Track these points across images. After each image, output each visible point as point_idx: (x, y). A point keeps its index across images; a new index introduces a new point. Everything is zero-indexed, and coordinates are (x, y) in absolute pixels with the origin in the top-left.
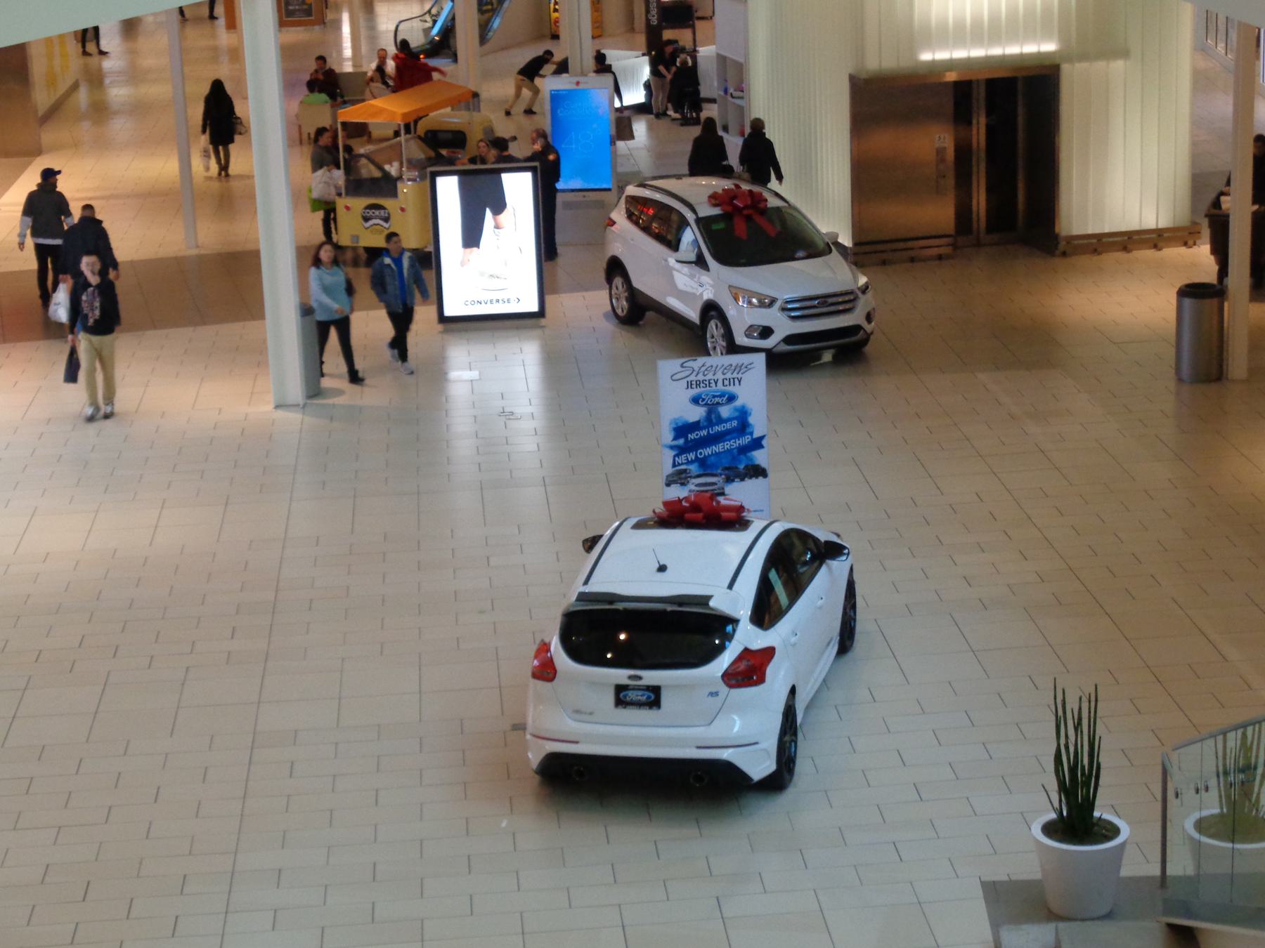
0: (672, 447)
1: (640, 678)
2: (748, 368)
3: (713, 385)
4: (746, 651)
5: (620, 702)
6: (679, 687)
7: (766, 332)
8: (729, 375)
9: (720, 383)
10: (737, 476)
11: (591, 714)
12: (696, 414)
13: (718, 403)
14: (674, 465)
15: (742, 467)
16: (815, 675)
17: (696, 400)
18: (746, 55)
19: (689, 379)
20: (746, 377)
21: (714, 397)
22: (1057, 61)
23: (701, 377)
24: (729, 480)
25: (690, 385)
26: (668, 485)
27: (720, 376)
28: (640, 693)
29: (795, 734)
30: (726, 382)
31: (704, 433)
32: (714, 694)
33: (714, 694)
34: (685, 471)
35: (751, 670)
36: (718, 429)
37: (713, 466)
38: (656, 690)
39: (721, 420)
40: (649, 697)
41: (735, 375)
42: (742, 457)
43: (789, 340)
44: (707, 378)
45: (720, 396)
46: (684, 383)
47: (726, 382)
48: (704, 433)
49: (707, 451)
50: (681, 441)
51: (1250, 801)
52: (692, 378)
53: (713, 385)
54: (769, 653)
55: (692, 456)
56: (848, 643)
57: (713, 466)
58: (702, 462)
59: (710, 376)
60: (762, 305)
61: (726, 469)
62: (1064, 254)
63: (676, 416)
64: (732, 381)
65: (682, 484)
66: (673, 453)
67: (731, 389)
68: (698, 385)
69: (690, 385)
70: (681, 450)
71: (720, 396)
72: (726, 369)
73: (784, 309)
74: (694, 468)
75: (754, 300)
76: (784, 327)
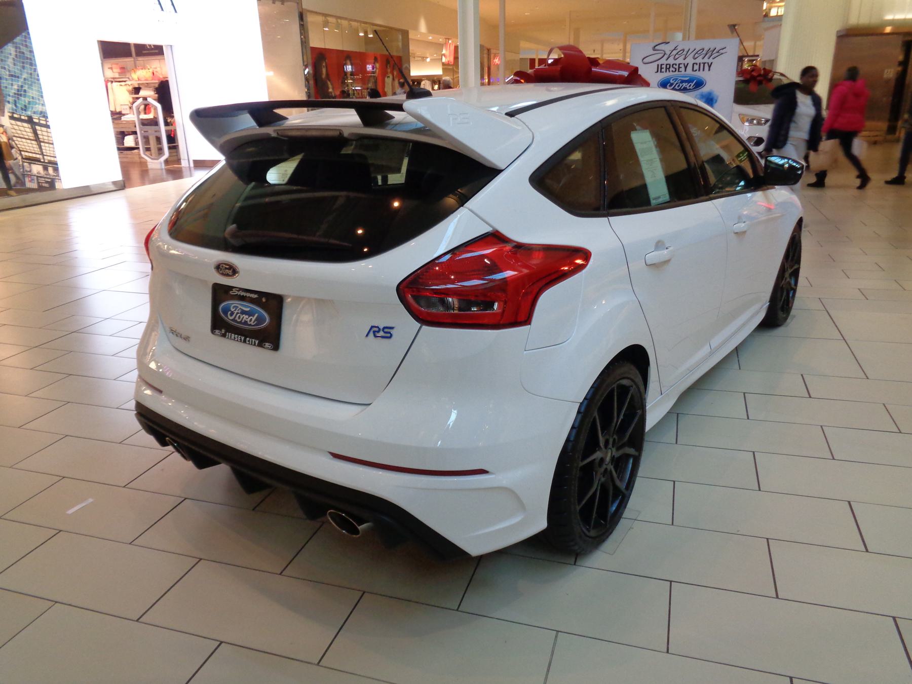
1: (231, 270)
2: (719, 52)
3: (683, 69)
4: (495, 237)
5: (220, 324)
6: (324, 304)
9: (690, 68)
11: (187, 339)
16: (715, 342)
18: (777, 57)
19: (660, 62)
20: (717, 63)
21: (682, 82)
23: (671, 61)
25: (659, 69)
27: (690, 60)
28: (247, 307)
29: (639, 449)
30: (696, 67)
32: (384, 333)
33: (384, 333)
35: (498, 291)
38: (273, 304)
40: (260, 320)
41: (706, 60)
44: (677, 62)
46: (655, 65)
47: (696, 67)
51: (500, 250)
52: (663, 61)
53: (683, 69)
54: (562, 262)
56: (781, 314)
59: (680, 60)
64: (702, 66)
67: (701, 75)
68: (667, 69)
72: (697, 53)
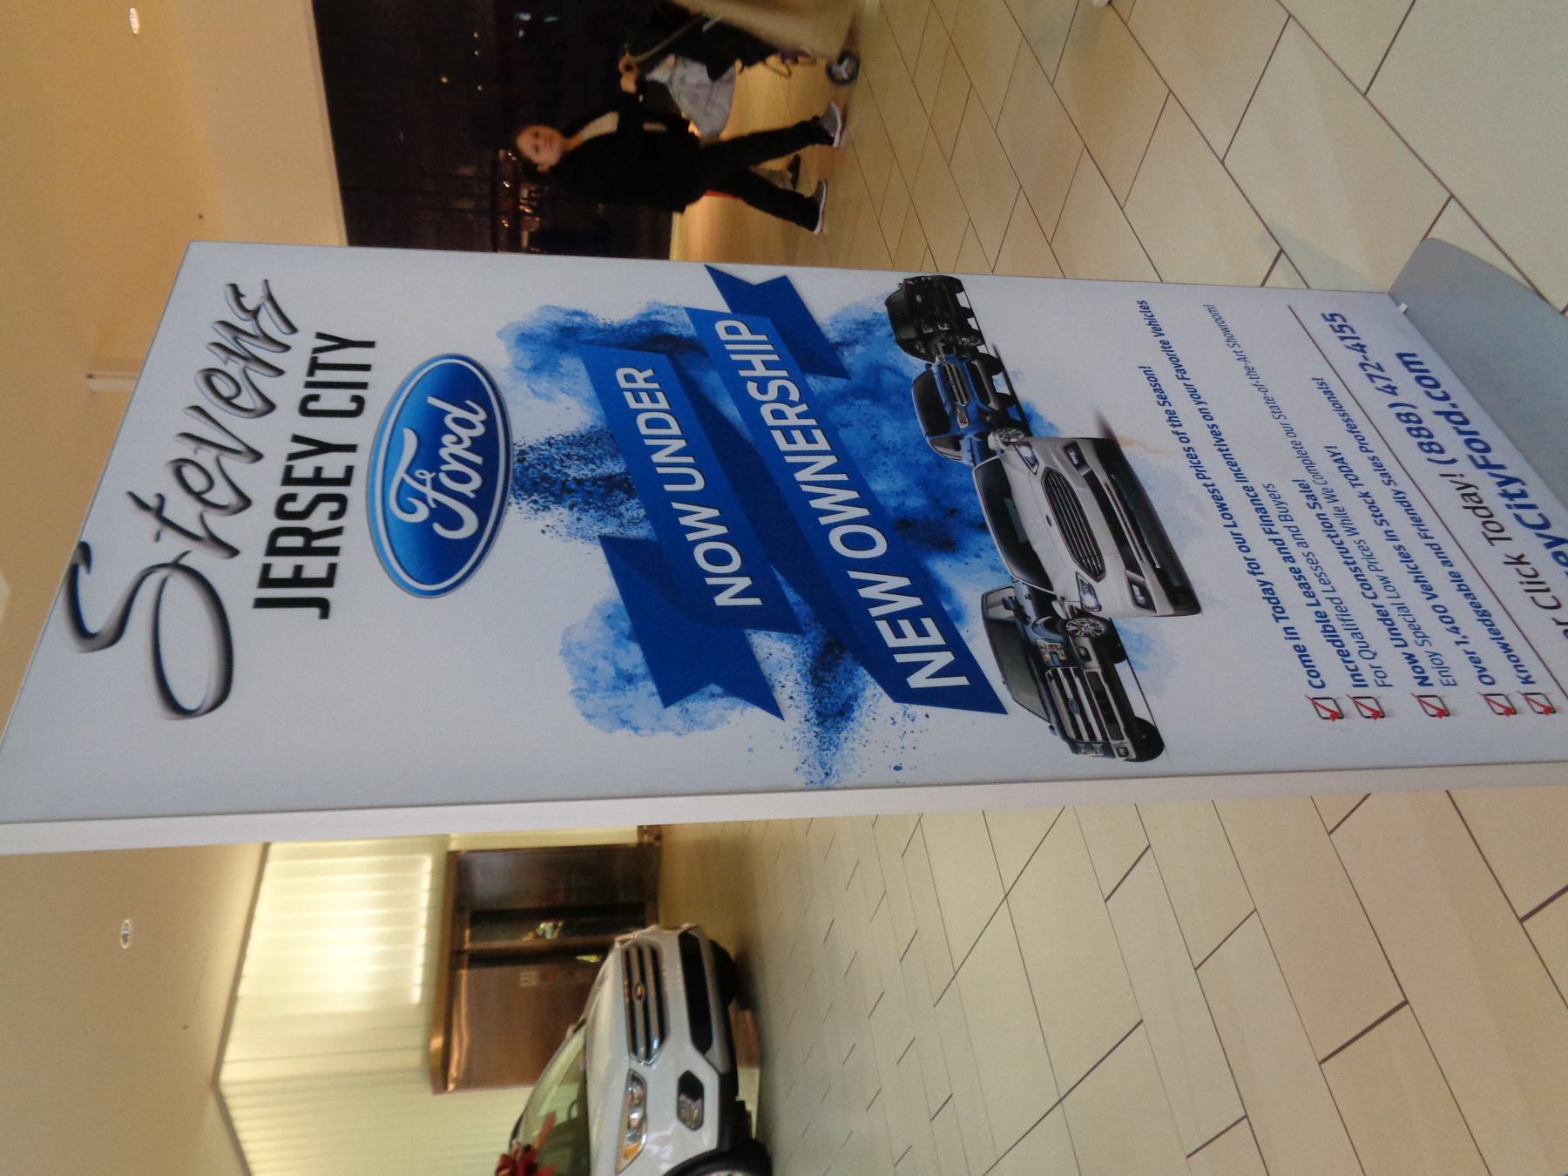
0: (833, 713)
3: (333, 465)
7: (690, 1086)
8: (288, 390)
10: (982, 390)
12: (549, 569)
13: (485, 445)
14: (979, 698)
15: (915, 366)
17: (439, 559)
21: (428, 457)
22: (443, 856)
24: (1013, 417)
25: (299, 590)
26: (1147, 742)
27: (274, 436)
31: (702, 525)
34: (1005, 634)
36: (669, 450)
37: (933, 479)
39: (616, 428)
41: (295, 363)
42: (851, 358)
43: (701, 1041)
45: (432, 431)
48: (702, 525)
49: (838, 511)
50: (776, 652)
53: (333, 465)
55: (885, 593)
57: (933, 479)
58: (920, 538)
59: (264, 483)
60: (641, 1102)
61: (939, 422)
62: (659, 838)
63: (562, 679)
65: (1111, 646)
66: (875, 703)
67: (384, 388)
69: (299, 590)
70: (849, 653)
71: (432, 431)
73: (648, 1056)
74: (975, 582)
75: (635, 1116)
76: (679, 1053)
